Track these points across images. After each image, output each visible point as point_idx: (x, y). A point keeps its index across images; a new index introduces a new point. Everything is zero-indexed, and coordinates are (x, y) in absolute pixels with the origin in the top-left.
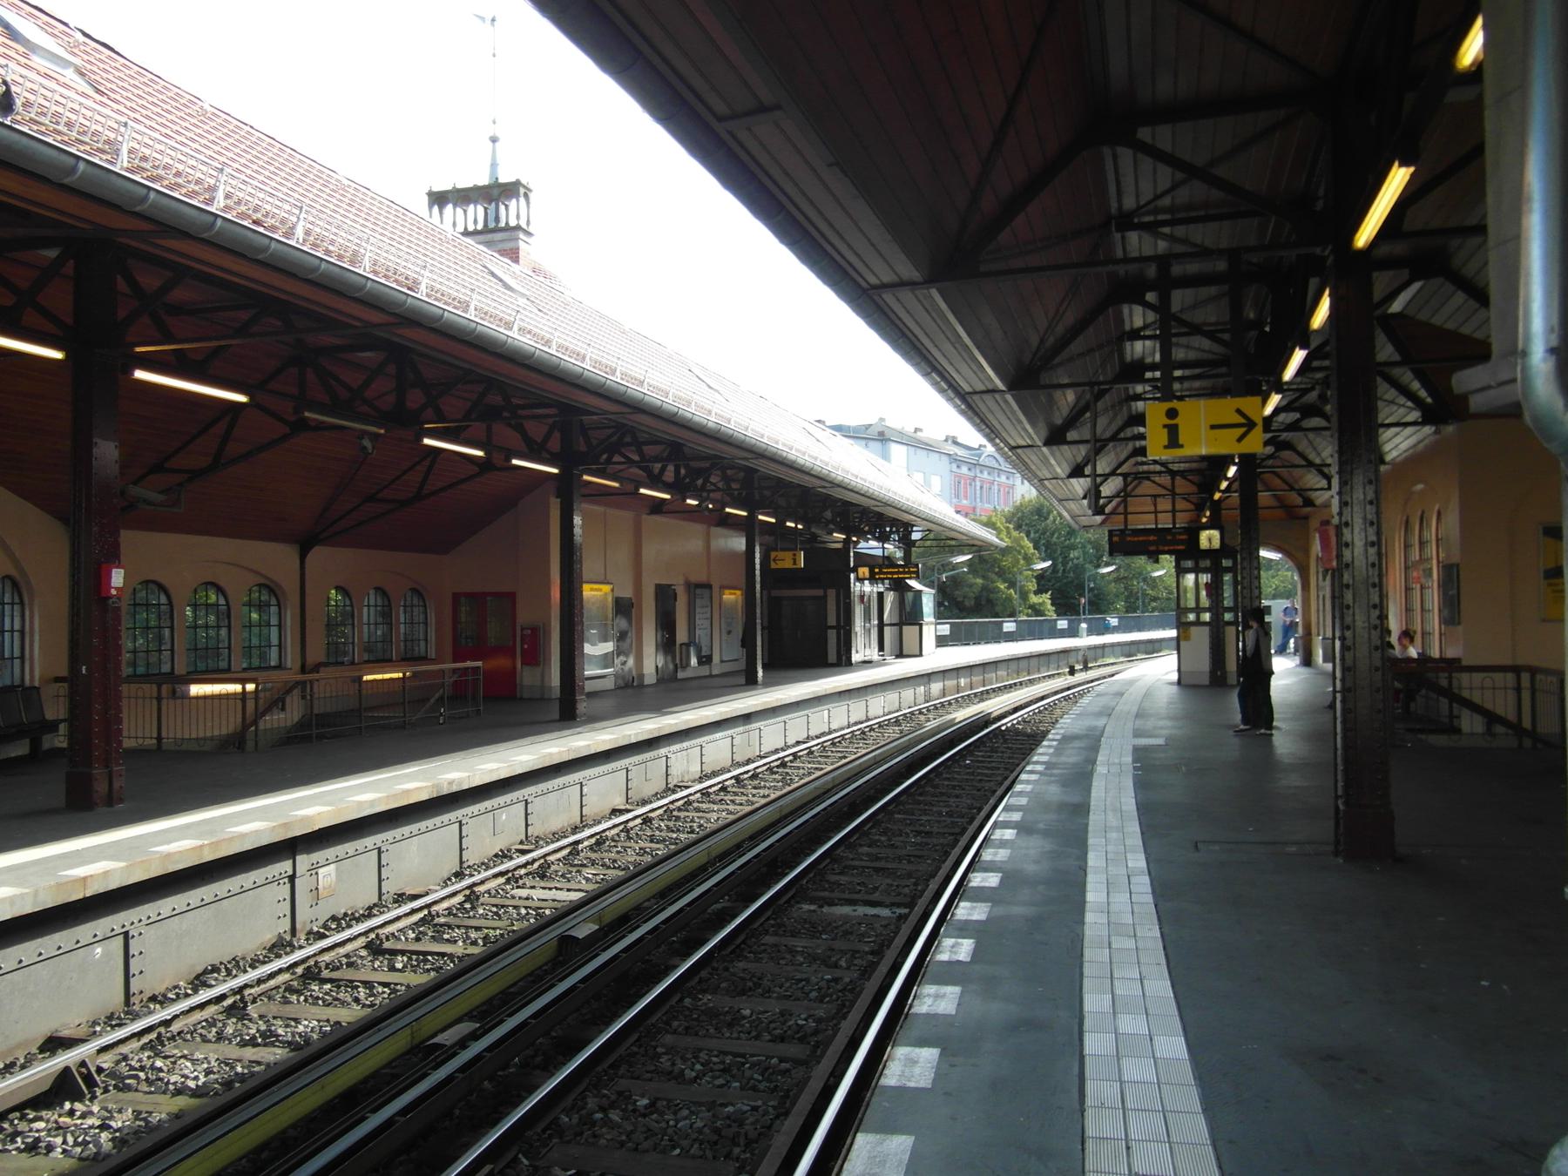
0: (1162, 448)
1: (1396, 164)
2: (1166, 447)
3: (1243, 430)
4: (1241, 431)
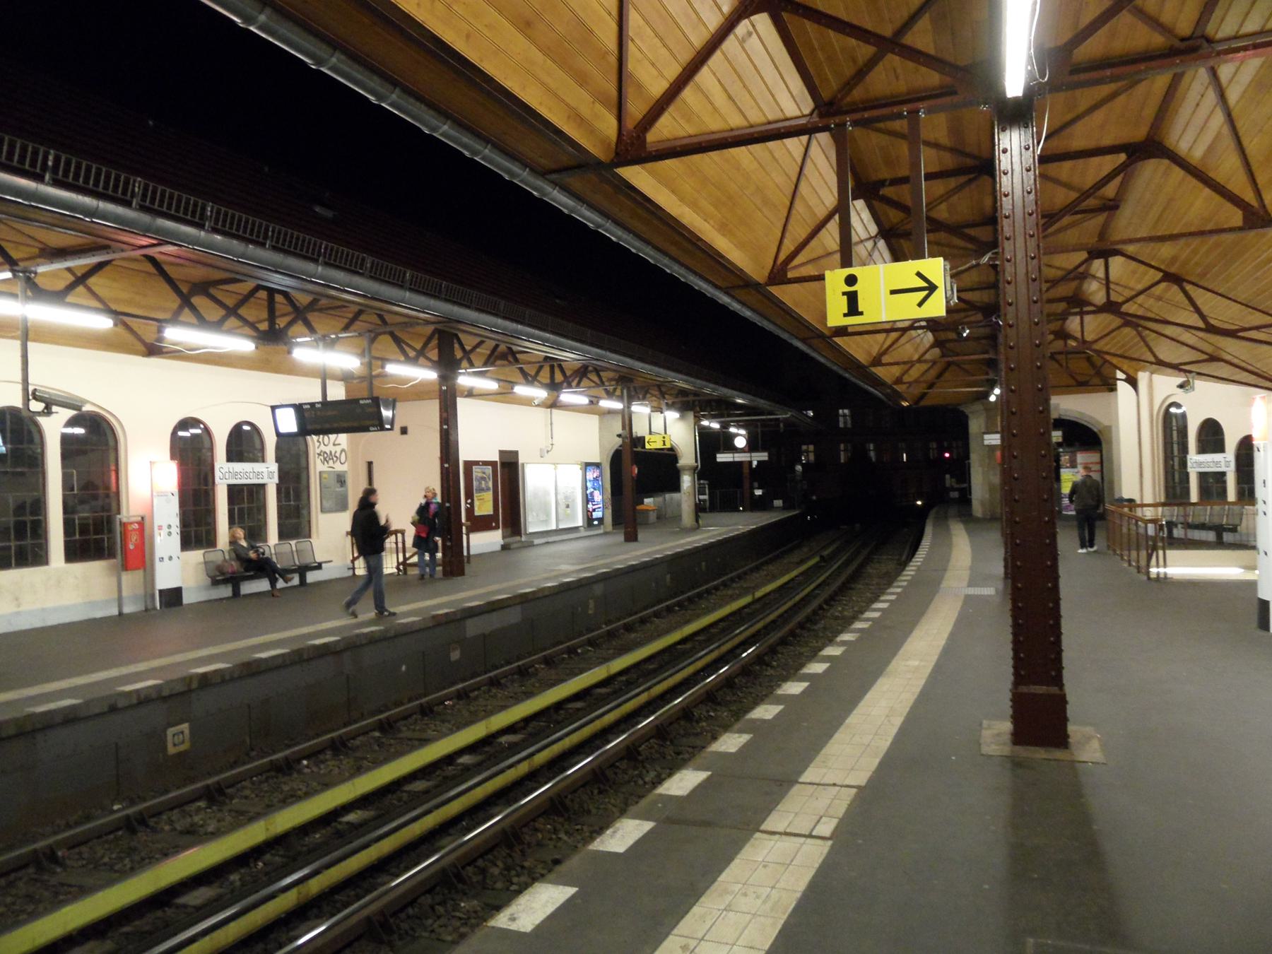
2: (845, 315)
3: (925, 293)
4: (921, 295)
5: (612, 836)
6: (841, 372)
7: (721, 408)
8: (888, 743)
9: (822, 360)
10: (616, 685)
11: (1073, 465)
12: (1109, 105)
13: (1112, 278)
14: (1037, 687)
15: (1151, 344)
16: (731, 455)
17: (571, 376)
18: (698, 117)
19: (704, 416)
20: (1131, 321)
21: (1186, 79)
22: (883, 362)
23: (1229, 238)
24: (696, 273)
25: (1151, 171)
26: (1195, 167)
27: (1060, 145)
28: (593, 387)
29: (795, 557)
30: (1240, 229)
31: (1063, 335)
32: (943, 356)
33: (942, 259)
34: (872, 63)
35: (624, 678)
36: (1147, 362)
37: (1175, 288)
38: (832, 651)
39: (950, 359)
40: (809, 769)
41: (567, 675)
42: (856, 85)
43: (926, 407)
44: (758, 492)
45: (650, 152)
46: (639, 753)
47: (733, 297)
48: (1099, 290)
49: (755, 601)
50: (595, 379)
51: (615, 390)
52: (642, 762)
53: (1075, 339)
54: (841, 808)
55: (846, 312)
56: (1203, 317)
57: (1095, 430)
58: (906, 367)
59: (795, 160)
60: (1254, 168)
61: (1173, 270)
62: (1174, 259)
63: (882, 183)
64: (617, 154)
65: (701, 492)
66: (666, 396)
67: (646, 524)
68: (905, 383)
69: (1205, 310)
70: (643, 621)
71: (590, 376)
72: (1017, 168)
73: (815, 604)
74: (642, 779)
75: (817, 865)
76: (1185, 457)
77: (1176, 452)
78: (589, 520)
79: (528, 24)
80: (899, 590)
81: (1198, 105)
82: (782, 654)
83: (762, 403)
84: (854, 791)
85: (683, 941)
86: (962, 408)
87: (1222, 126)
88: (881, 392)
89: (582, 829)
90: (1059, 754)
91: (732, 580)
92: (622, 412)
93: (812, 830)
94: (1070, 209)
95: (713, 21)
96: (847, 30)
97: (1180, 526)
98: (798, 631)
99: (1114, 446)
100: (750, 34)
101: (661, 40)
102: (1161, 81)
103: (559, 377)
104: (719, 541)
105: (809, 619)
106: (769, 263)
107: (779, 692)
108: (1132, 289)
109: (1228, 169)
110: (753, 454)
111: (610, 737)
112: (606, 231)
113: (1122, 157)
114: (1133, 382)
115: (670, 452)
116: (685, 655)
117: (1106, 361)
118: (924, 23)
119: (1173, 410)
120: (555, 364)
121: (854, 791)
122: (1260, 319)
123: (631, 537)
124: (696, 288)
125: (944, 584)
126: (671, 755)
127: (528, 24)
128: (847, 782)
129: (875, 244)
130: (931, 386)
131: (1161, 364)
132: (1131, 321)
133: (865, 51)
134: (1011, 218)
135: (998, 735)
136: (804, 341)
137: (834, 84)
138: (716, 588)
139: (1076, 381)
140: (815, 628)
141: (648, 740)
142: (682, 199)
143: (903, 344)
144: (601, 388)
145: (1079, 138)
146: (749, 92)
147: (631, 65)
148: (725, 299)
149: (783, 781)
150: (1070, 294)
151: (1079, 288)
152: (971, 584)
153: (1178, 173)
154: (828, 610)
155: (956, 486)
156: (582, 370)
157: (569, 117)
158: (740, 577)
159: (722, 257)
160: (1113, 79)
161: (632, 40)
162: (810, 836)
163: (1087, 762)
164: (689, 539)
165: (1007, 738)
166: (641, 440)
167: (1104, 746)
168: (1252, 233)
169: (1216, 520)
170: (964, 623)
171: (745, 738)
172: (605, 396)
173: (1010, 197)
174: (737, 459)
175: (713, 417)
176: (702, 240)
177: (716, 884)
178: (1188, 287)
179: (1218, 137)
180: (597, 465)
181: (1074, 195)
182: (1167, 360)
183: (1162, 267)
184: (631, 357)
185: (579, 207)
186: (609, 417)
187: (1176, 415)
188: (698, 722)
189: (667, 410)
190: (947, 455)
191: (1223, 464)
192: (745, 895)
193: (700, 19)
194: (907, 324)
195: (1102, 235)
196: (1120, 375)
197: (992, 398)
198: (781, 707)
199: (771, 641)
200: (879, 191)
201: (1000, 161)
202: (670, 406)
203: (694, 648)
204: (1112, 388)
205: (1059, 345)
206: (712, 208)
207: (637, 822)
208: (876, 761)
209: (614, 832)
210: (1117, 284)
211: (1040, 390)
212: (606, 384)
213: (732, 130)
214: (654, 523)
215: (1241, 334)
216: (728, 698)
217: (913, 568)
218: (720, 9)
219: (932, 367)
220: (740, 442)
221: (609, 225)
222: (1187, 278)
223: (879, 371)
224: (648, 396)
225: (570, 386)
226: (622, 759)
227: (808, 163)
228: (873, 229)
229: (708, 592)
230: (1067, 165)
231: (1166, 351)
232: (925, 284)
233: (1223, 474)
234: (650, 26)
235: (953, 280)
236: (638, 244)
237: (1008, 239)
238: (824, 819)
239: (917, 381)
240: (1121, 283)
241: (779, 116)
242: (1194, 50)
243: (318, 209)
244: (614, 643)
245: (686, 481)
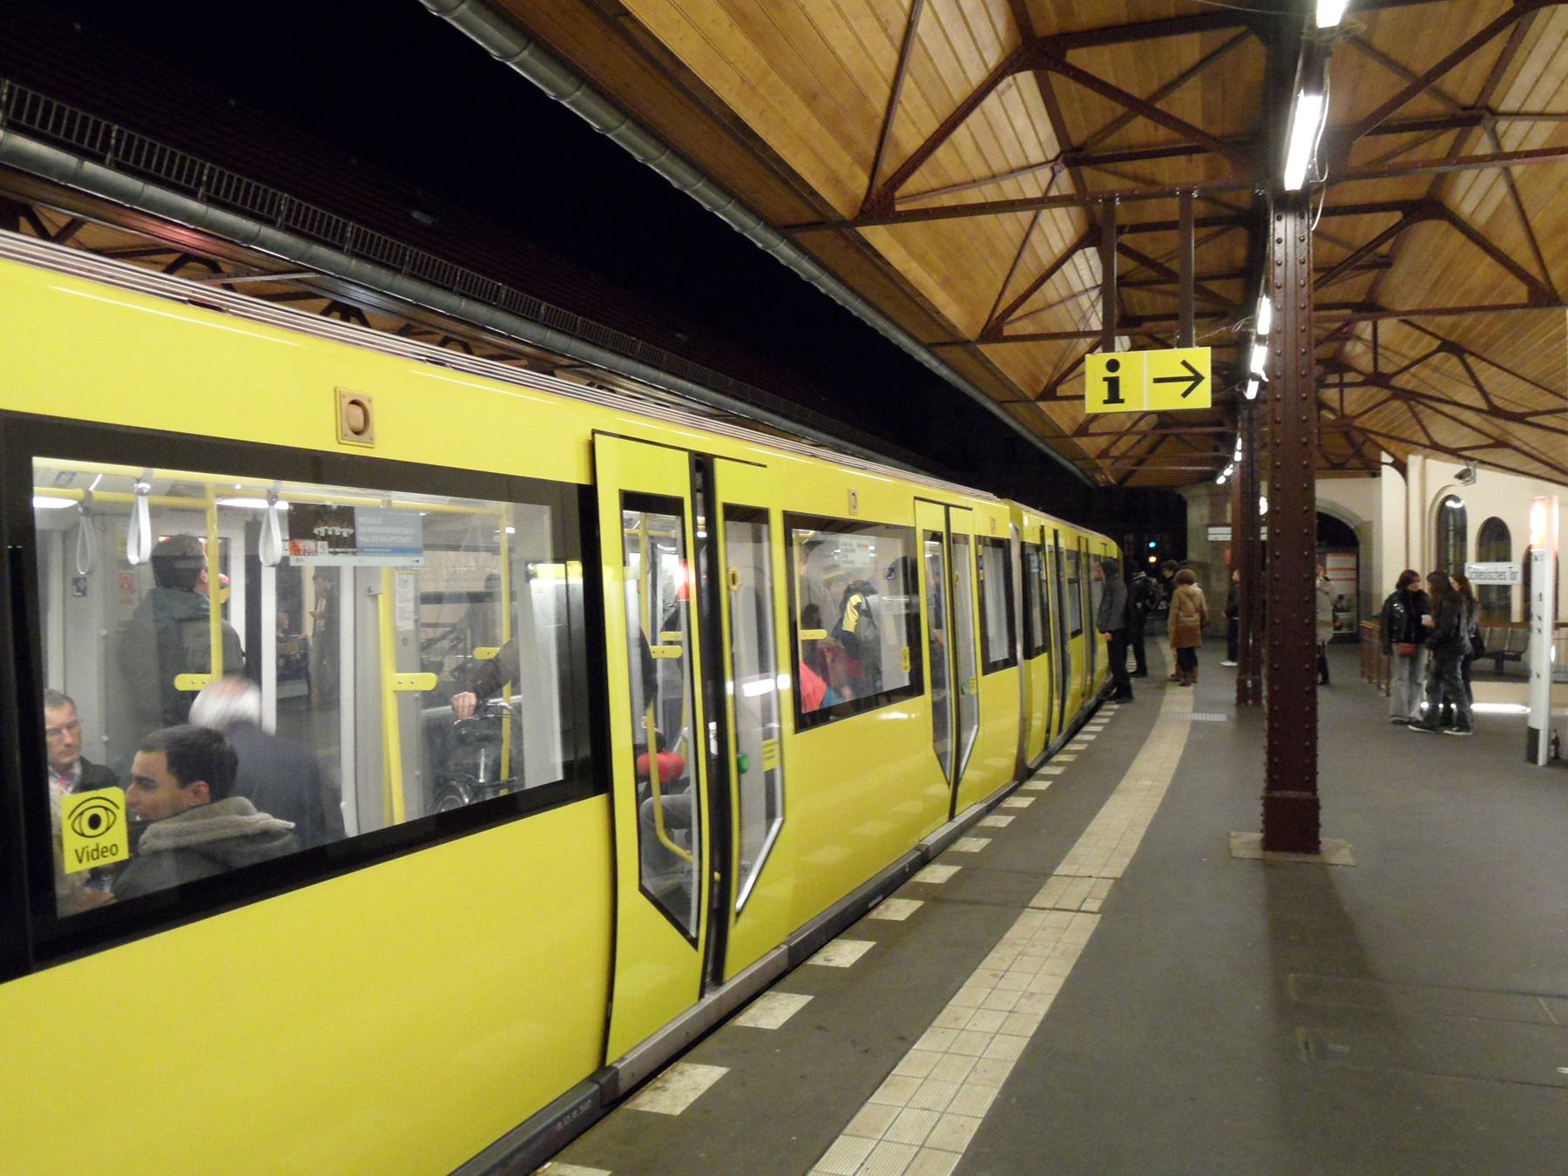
1: (1302, 91)
2: (1106, 402)
8: (1136, 846)
13: (1381, 340)
14: (1290, 792)
25: (1430, 232)
26: (1478, 233)
30: (1524, 306)
33: (1209, 348)
36: (1420, 445)
37: (1455, 359)
47: (934, 355)
48: (1365, 353)
53: (1331, 409)
55: (1106, 398)
56: (1485, 395)
57: (1352, 527)
58: (1114, 438)
61: (1452, 338)
64: (862, 211)
79: (814, 97)
80: (1099, 729)
86: (1179, 491)
87: (1505, 197)
90: (1312, 858)
95: (977, 76)
108: (1404, 356)
109: (1511, 239)
113: (1397, 216)
114: (1401, 467)
119: (1450, 504)
121: (1111, 881)
122: (1552, 402)
127: (814, 97)
128: (1103, 874)
131: (1436, 448)
142: (911, 254)
151: (1340, 350)
152: (1195, 710)
153: (1458, 238)
157: (827, 180)
162: (1079, 911)
163: (1337, 865)
165: (1258, 845)
168: (1536, 312)
171: (952, 870)
176: (922, 295)
178: (1470, 360)
179: (1501, 207)
183: (1441, 334)
185: (800, 260)
187: (1453, 510)
191: (1507, 575)
196: (1386, 458)
197: (1221, 480)
204: (1375, 472)
208: (1127, 861)
215: (1530, 419)
223: (1084, 443)
238: (1088, 900)
239: (1124, 456)
240: (1391, 347)
243: (416, 215)
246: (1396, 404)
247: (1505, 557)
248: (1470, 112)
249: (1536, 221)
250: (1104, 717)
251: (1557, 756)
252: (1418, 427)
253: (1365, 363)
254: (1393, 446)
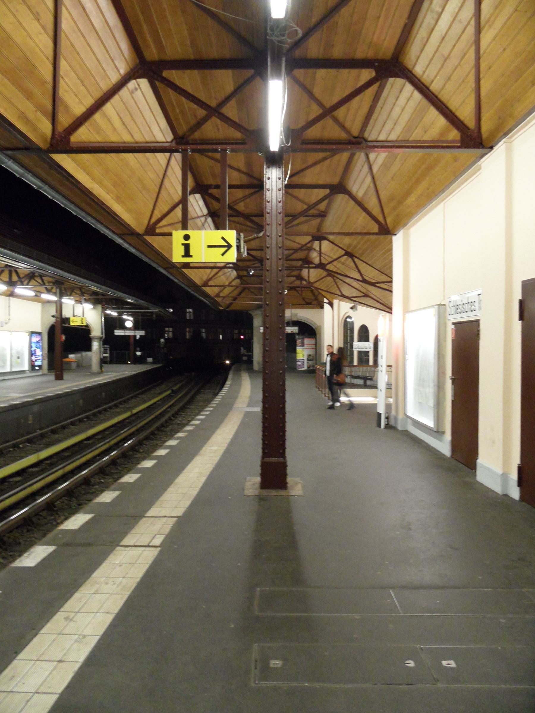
0: (181, 256)
3: (226, 248)
4: (225, 249)
5: (27, 557)
6: (186, 288)
7: (118, 304)
9: (176, 280)
10: (43, 465)
11: (303, 345)
12: (321, 164)
15: (340, 286)
16: (123, 331)
17: (23, 278)
18: (104, 132)
19: (108, 308)
20: (331, 274)
21: (356, 158)
22: (209, 284)
23: (373, 237)
24: (102, 224)
25: (340, 199)
26: (359, 201)
27: (297, 180)
28: (37, 286)
29: (158, 390)
31: (300, 278)
32: (241, 284)
34: (204, 120)
35: (48, 462)
37: (350, 259)
38: (172, 443)
39: (245, 286)
40: (152, 509)
41: (11, 461)
42: (196, 130)
43: (231, 311)
44: (139, 353)
45: (72, 148)
46: (55, 506)
49: (133, 415)
50: (40, 281)
51: (52, 288)
52: (57, 511)
53: (305, 280)
54: (167, 529)
56: (361, 275)
57: (314, 327)
59: (162, 166)
60: (383, 205)
61: (349, 250)
62: (350, 245)
63: (210, 186)
64: (51, 145)
65: (105, 352)
66: (85, 295)
67: (69, 369)
68: (220, 297)
69: (362, 271)
70: (63, 427)
71: (36, 279)
72: (274, 188)
73: (166, 417)
74: (56, 521)
75: (150, 562)
76: (352, 343)
77: (349, 341)
78: (33, 367)
80: (211, 409)
81: (361, 170)
82: (146, 445)
83: (141, 302)
84: (175, 519)
85: (66, 614)
86: (250, 312)
88: (208, 301)
89: (14, 555)
90: (282, 493)
91: (120, 403)
92: (55, 302)
93: (150, 543)
94: (304, 213)
95: (114, 78)
96: (191, 98)
97: (349, 377)
98: (156, 432)
99: (322, 335)
100: (136, 89)
101: (82, 82)
102: (345, 156)
103: (15, 278)
104: (114, 380)
105: (162, 425)
106: (146, 222)
107: (140, 466)
109: (372, 204)
110: (137, 331)
111: (37, 497)
112: (44, 191)
114: (331, 304)
115: (86, 328)
116: (89, 446)
117: (320, 293)
118: (233, 103)
119: (348, 320)
120: (12, 269)
123: (59, 377)
124: (102, 232)
125: (235, 406)
126: (75, 506)
129: (206, 219)
130: (235, 299)
132: (331, 274)
133: (201, 112)
134: (270, 214)
135: (254, 484)
136: (165, 269)
137: (185, 128)
138: (110, 408)
139: (306, 302)
140: (165, 430)
141: (61, 498)
142: (93, 179)
143: (220, 276)
144: (43, 287)
145: (309, 178)
146: (135, 123)
147: (62, 92)
148: (119, 241)
149: (136, 517)
150: (304, 258)
152: (249, 405)
153: (352, 203)
154: (173, 420)
155: (246, 353)
156: (31, 275)
157: (19, 117)
158: (125, 402)
159: (117, 216)
160: (322, 150)
161: (62, 78)
162: (149, 546)
163: (294, 496)
164: (95, 379)
165: (258, 486)
166: (67, 320)
167: (304, 487)
169: (364, 375)
170: (243, 425)
171: (116, 493)
172: (45, 292)
173: (270, 203)
174: (126, 334)
175: (113, 309)
177: (91, 579)
178: (356, 260)
179: (369, 187)
180: (39, 334)
181: (305, 207)
182: (346, 295)
183: (345, 248)
184: (62, 269)
186: (48, 304)
187: (349, 322)
188: (93, 486)
189: (85, 303)
190: (242, 337)
192: (107, 583)
193: (106, 75)
194: (222, 265)
195: (319, 229)
196: (326, 300)
198: (139, 475)
199: (141, 437)
200: (208, 190)
201: (266, 184)
202: (87, 301)
203: (94, 442)
204: (322, 307)
205: (298, 283)
206: (112, 187)
207: (45, 547)
209: (29, 555)
210: (325, 254)
211: (281, 305)
212: (47, 284)
213: (124, 143)
214: (74, 369)
215: (377, 285)
216: (113, 471)
217: (221, 397)
218: (118, 71)
219: (235, 289)
220: (129, 324)
221: (46, 187)
222: (355, 255)
223: (207, 290)
224: (74, 294)
225: (22, 283)
226: (43, 510)
227: (169, 169)
228: (205, 211)
229: (105, 410)
230: (303, 190)
231: (346, 291)
232: (226, 244)
233: (368, 352)
234: (74, 72)
235: (245, 244)
236: (65, 202)
237: (268, 225)
239: (227, 296)
241: (153, 140)
242: (359, 143)
244: (44, 441)
245: (95, 345)
246: (329, 278)
247: (367, 339)
248: (356, 139)
249: (382, 196)
250: (214, 404)
251: (388, 424)
252: (337, 288)
253: (317, 261)
254: (328, 295)
